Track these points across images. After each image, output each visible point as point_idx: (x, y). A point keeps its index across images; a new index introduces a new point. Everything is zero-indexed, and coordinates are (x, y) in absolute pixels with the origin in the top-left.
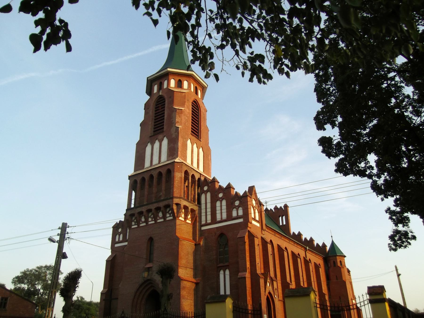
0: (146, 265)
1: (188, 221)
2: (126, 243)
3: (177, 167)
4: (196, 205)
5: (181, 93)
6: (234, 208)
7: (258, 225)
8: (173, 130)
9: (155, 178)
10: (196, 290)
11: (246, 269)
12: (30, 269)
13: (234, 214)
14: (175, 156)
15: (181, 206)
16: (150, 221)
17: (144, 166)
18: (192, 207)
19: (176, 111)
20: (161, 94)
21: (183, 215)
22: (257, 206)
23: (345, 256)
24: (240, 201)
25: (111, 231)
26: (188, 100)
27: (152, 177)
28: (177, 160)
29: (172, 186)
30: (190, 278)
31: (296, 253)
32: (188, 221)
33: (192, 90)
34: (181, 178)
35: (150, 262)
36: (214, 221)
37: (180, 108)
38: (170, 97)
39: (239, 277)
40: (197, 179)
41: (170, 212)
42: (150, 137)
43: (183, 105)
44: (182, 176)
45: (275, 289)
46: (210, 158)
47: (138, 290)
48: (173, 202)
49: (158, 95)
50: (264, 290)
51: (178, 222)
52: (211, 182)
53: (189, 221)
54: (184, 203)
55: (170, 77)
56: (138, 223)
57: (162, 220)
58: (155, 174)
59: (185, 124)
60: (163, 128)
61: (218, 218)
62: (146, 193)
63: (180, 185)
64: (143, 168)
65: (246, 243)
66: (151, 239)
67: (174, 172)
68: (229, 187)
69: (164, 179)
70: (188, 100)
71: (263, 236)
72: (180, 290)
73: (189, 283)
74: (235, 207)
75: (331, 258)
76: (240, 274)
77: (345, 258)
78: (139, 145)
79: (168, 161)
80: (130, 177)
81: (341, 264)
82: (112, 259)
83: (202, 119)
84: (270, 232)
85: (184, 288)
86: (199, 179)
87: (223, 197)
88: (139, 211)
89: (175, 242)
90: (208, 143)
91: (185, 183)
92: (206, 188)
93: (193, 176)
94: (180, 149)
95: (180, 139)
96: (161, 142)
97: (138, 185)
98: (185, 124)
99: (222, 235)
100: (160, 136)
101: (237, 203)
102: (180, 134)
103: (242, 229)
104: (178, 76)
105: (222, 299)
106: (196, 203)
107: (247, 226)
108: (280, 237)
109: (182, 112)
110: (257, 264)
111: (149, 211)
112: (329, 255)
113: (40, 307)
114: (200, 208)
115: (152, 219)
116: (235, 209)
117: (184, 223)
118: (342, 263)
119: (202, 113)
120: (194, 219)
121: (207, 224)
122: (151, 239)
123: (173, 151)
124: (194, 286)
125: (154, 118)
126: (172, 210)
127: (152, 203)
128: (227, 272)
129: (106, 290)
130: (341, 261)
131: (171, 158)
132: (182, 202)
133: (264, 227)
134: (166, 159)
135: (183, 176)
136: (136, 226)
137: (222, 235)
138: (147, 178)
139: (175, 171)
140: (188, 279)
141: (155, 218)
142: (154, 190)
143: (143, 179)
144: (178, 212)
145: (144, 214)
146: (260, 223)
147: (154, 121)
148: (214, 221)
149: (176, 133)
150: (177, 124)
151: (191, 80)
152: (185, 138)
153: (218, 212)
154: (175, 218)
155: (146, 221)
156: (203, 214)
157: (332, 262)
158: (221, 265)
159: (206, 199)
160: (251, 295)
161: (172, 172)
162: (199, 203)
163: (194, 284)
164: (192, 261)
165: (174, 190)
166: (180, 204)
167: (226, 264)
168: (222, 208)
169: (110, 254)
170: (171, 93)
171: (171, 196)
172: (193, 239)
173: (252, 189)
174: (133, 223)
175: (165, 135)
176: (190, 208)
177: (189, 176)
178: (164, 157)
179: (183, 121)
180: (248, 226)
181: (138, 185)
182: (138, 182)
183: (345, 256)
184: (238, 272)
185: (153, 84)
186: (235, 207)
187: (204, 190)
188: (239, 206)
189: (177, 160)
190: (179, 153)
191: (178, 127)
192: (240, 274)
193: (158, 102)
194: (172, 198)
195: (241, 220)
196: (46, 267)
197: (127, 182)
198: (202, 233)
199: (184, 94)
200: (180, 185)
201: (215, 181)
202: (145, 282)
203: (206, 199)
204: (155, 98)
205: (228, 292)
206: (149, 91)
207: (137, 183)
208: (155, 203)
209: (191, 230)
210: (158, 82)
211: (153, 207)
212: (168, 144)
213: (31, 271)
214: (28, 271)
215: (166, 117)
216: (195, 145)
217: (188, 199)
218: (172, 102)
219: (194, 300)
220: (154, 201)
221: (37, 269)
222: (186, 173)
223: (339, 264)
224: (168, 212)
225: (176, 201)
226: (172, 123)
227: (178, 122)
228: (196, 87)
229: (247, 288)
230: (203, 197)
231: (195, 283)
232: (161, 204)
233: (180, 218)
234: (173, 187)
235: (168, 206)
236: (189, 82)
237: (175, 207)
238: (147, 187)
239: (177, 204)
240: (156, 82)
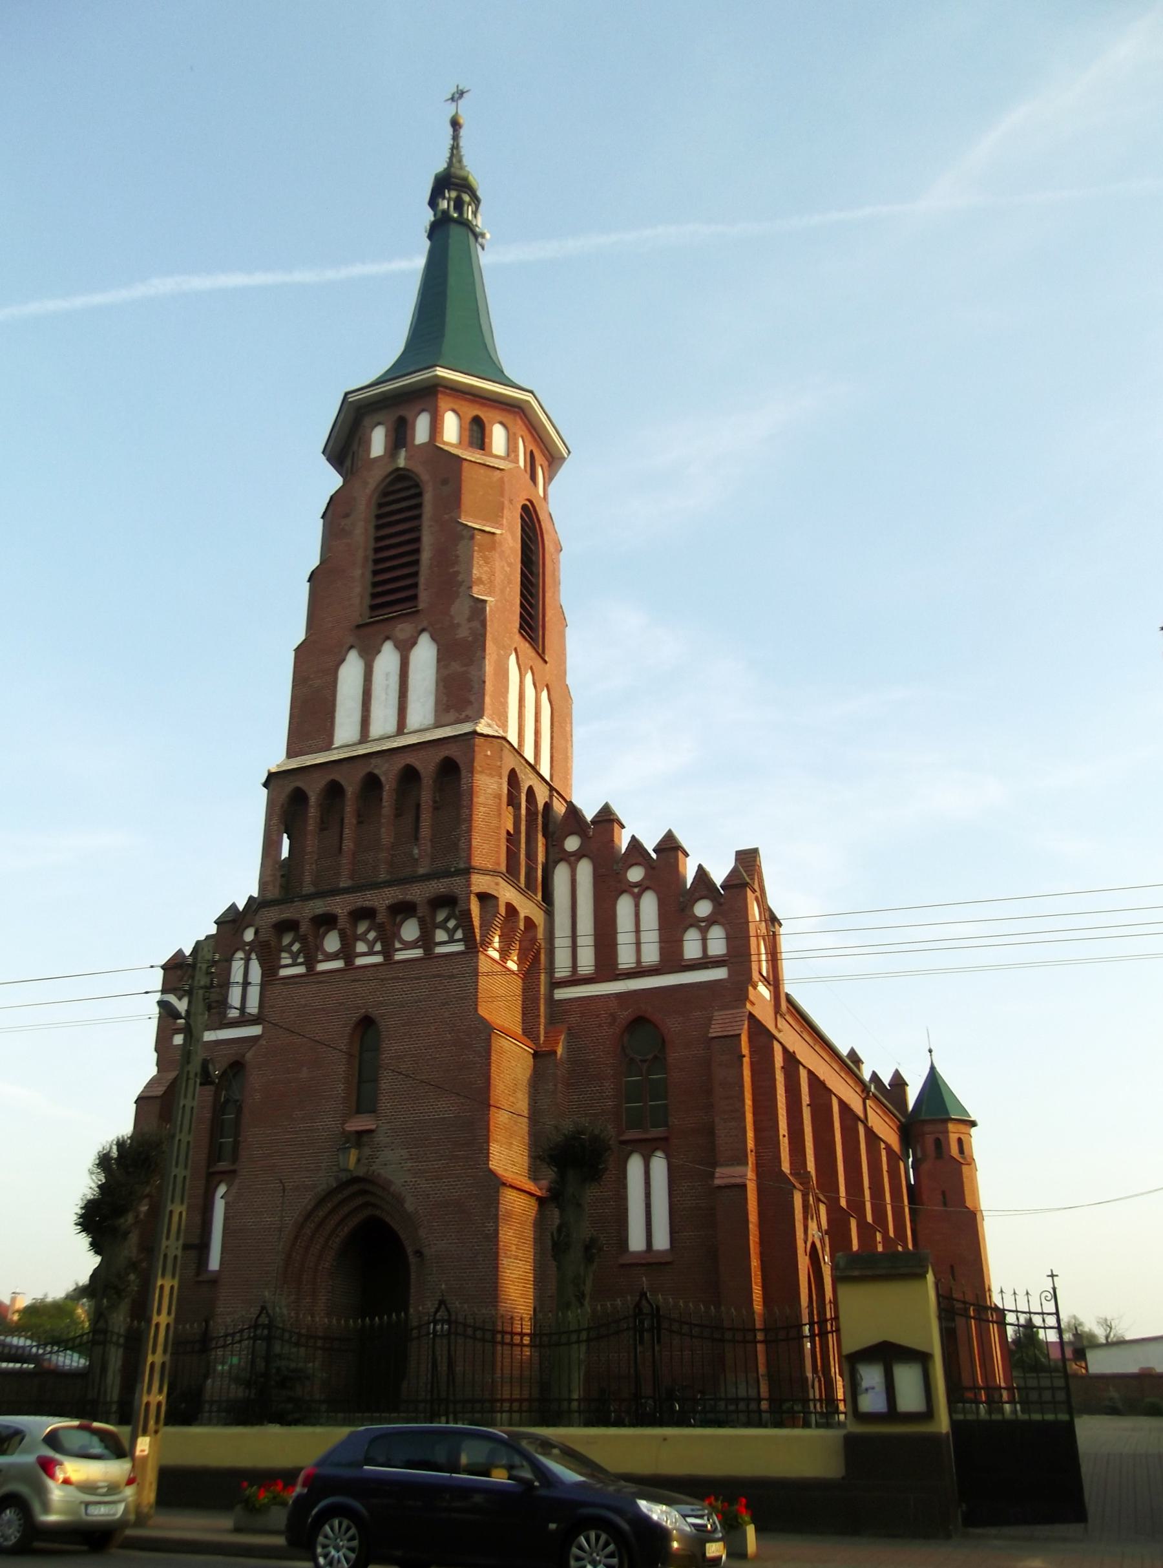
2: (255, 1030)
3: (483, 753)
5: (489, 472)
8: (460, 610)
9: (387, 787)
10: (540, 1224)
11: (746, 1156)
13: (691, 949)
14: (469, 712)
15: (497, 906)
17: (332, 743)
19: (472, 537)
20: (401, 462)
23: (973, 1124)
26: (511, 501)
27: (372, 783)
30: (521, 1178)
33: (522, 463)
34: (499, 797)
35: (359, 1111)
36: (606, 968)
37: (488, 529)
38: (445, 482)
39: (717, 1182)
41: (451, 924)
42: (359, 627)
44: (501, 789)
46: (568, 729)
47: (309, 1216)
48: (469, 886)
49: (390, 469)
51: (484, 965)
53: (512, 965)
55: (443, 402)
57: (338, 964)
58: (388, 774)
59: (502, 591)
60: (415, 597)
61: (626, 958)
64: (328, 746)
66: (367, 1023)
67: (472, 771)
68: (670, 847)
70: (511, 501)
73: (523, 1196)
74: (695, 922)
75: (928, 1128)
76: (719, 1171)
77: (973, 1131)
79: (438, 725)
80: (272, 780)
81: (961, 1151)
82: (165, 1092)
83: (548, 580)
88: (319, 911)
92: (572, 844)
94: (489, 687)
96: (405, 649)
98: (502, 591)
99: (641, 1027)
100: (403, 629)
103: (723, 1007)
104: (472, 401)
106: (539, 897)
109: (494, 542)
111: (359, 914)
112: (923, 1117)
114: (549, 913)
116: (240, 955)
117: (498, 968)
118: (965, 1147)
119: (547, 556)
121: (575, 980)
122: (367, 1023)
123: (461, 690)
126: (468, 914)
128: (659, 1165)
130: (960, 1141)
131: (452, 716)
134: (429, 720)
135: (505, 791)
137: (639, 1022)
138: (351, 786)
139: (477, 765)
141: (388, 940)
143: (334, 791)
144: (486, 926)
148: (606, 968)
149: (476, 624)
151: (519, 427)
154: (473, 947)
155: (347, 953)
157: (929, 1140)
158: (630, 1135)
160: (758, 1251)
161: (464, 773)
162: (548, 898)
165: (474, 843)
166: (496, 898)
168: (639, 923)
170: (448, 466)
171: (462, 866)
172: (525, 1032)
173: (748, 860)
175: (425, 624)
177: (520, 794)
178: (421, 711)
179: (495, 582)
182: (313, 799)
183: (973, 1124)
185: (367, 422)
186: (695, 922)
188: (711, 921)
189: (482, 728)
190: (487, 699)
191: (485, 601)
192: (724, 1175)
194: (468, 871)
195: (720, 974)
201: (613, 821)
202: (343, 1185)
203: (576, 884)
204: (374, 479)
206: (343, 448)
207: (292, 800)
208: (389, 884)
210: (392, 416)
211: (381, 899)
212: (439, 660)
215: (426, 556)
216: (529, 678)
218: (453, 500)
220: (383, 876)
222: (513, 775)
223: (954, 1151)
224: (443, 926)
225: (480, 883)
226: (453, 582)
227: (480, 581)
228: (532, 452)
230: (561, 874)
234: (469, 830)
235: (449, 901)
236: (512, 430)
237: (475, 907)
239: (484, 898)
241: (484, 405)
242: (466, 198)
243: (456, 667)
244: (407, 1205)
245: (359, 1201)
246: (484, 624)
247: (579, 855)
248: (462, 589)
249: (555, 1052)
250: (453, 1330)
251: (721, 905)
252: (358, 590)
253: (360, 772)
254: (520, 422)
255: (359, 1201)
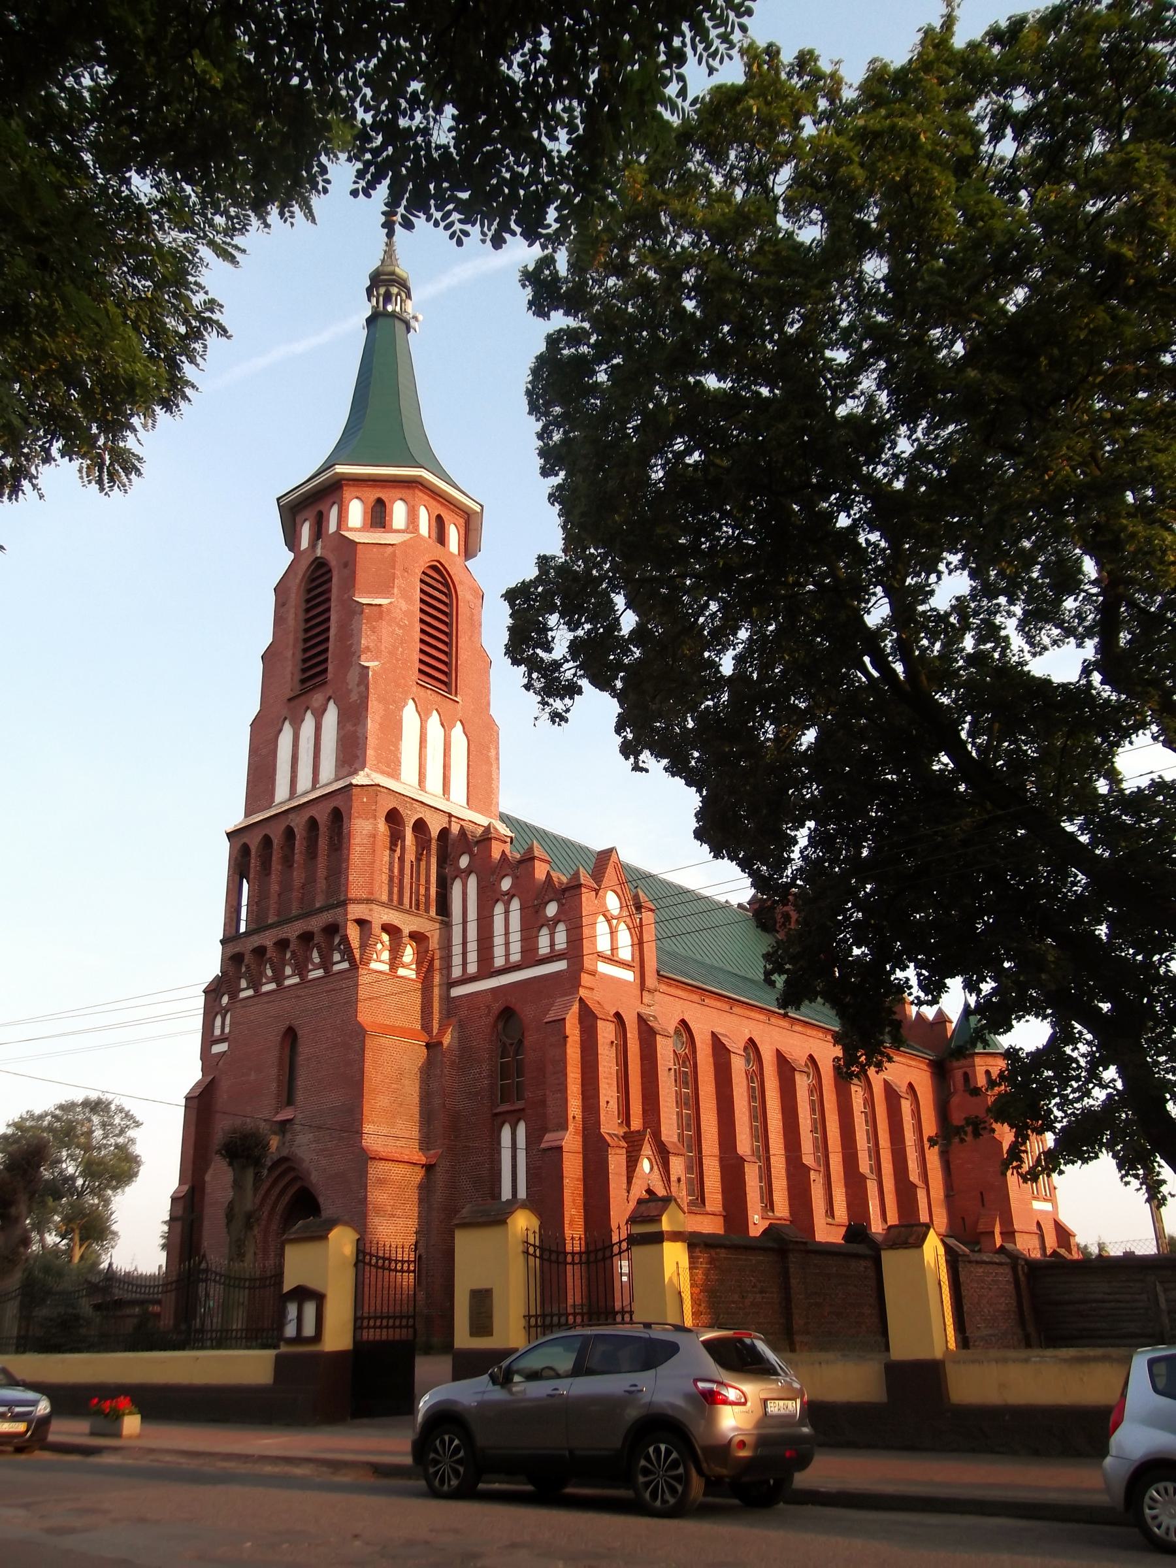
0: (277, 1113)
1: (402, 972)
3: (360, 801)
4: (431, 919)
5: (381, 549)
6: (542, 926)
7: (628, 976)
8: (353, 676)
9: (298, 837)
10: (425, 1190)
12: (37, 1112)
13: (543, 942)
14: (356, 766)
16: (289, 977)
18: (414, 928)
19: (362, 612)
20: (319, 553)
21: (386, 956)
22: (625, 913)
24: (558, 901)
25: (200, 1001)
26: (405, 570)
27: (313, 824)
28: (360, 779)
29: (344, 865)
31: (911, 983)
32: (402, 972)
36: (487, 969)
38: (346, 565)
39: (543, 1146)
40: (435, 832)
42: (290, 700)
43: (385, 588)
44: (375, 828)
45: (673, 1178)
50: (625, 1186)
51: (364, 978)
52: (478, 842)
53: (410, 973)
54: (381, 916)
55: (347, 492)
56: (255, 984)
57: (272, 986)
58: (298, 823)
59: (392, 653)
60: (325, 670)
61: (499, 962)
62: (275, 888)
63: (368, 858)
65: (569, 1040)
66: (291, 1036)
69: (323, 843)
71: (645, 1011)
72: (366, 1189)
78: (257, 726)
79: (337, 779)
84: (680, 993)
85: (381, 1182)
86: (444, 832)
87: (513, 891)
88: (256, 945)
89: (354, 1040)
90: (489, 704)
91: (393, 850)
93: (420, 826)
94: (372, 741)
95: (374, 705)
96: (319, 716)
97: (254, 862)
99: (507, 1013)
100: (317, 698)
101: (552, 910)
102: (371, 690)
105: (498, 1218)
106: (433, 912)
107: (576, 984)
108: (727, 1007)
109: (381, 612)
110: (602, 1104)
111: (306, 938)
113: (77, 1231)
114: (447, 925)
115: (342, 957)
116: (545, 931)
120: (424, 961)
121: (466, 980)
122: (291, 1036)
123: (351, 752)
124: (418, 1175)
125: (302, 636)
126: (345, 940)
127: (289, 921)
128: (521, 1129)
129: (186, 1188)
130: (966, 1075)
132: (375, 915)
133: (651, 981)
134: (332, 776)
136: (250, 992)
137: (507, 1014)
140: (397, 1156)
142: (298, 876)
143: (267, 841)
145: (246, 961)
146: (637, 969)
147: (301, 646)
149: (362, 688)
150: (363, 657)
152: (394, 701)
153: (499, 940)
155: (278, 978)
156: (457, 950)
158: (505, 1107)
159: (465, 895)
160: (580, 1201)
162: (444, 908)
163: (417, 1169)
164: (416, 1099)
165: (351, 878)
166: (370, 922)
167: (519, 1105)
168: (508, 921)
169: (199, 1075)
174: (243, 984)
175: (330, 693)
176: (406, 932)
178: (328, 770)
180: (580, 985)
181: (254, 862)
182: (275, 842)
184: (545, 1130)
185: (299, 519)
187: (459, 868)
188: (556, 921)
189: (360, 779)
190: (370, 753)
191: (368, 667)
193: (314, 580)
194: (344, 904)
195: (561, 965)
196: (86, 1104)
197: (222, 851)
198: (451, 1006)
199: (390, 549)
200: (368, 858)
203: (465, 895)
204: (305, 563)
205: (522, 1194)
208: (297, 918)
209: (416, 999)
210: (311, 513)
211: (292, 932)
213: (41, 1117)
214: (32, 1116)
216: (434, 721)
217: (401, 902)
218: (350, 583)
219: (419, 1217)
220: (294, 912)
221: (58, 1112)
222: (393, 817)
226: (350, 654)
227: (368, 648)
228: (439, 518)
229: (566, 1181)
230: (456, 889)
231: (423, 1166)
232: (315, 924)
233: (374, 965)
235: (333, 929)
236: (412, 503)
237: (353, 933)
238: (276, 865)
239: (362, 923)
240: (306, 514)
241: (383, 487)
242: (394, 290)
243: (349, 727)
244: (312, 1177)
245: (287, 1179)
246: (367, 688)
247: (469, 871)
248: (355, 658)
249: (441, 1043)
250: (592, 1259)
251: (563, 905)
252: (289, 669)
253: (280, 827)
254: (421, 494)
255: (287, 1179)
